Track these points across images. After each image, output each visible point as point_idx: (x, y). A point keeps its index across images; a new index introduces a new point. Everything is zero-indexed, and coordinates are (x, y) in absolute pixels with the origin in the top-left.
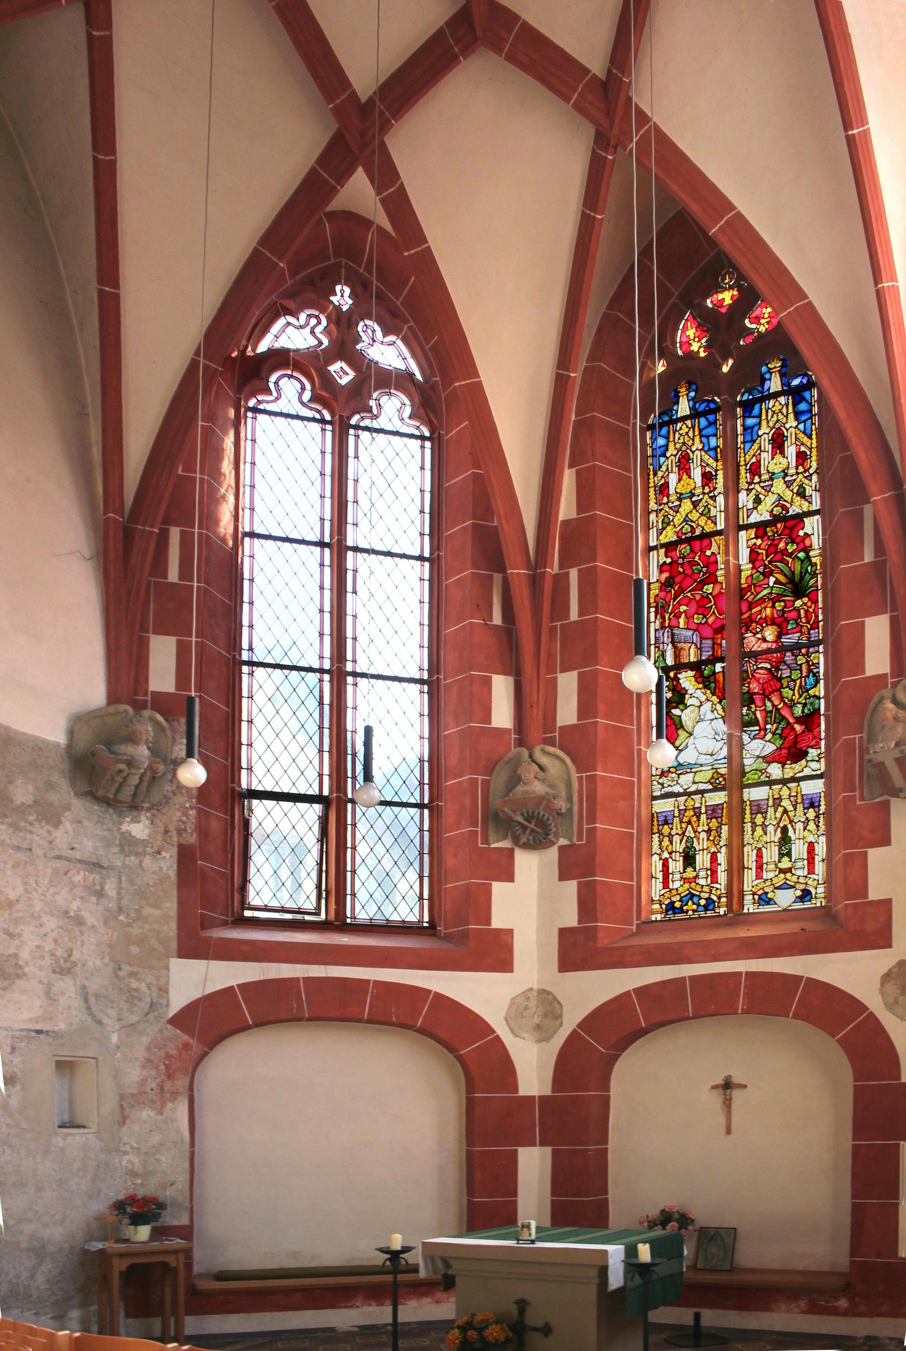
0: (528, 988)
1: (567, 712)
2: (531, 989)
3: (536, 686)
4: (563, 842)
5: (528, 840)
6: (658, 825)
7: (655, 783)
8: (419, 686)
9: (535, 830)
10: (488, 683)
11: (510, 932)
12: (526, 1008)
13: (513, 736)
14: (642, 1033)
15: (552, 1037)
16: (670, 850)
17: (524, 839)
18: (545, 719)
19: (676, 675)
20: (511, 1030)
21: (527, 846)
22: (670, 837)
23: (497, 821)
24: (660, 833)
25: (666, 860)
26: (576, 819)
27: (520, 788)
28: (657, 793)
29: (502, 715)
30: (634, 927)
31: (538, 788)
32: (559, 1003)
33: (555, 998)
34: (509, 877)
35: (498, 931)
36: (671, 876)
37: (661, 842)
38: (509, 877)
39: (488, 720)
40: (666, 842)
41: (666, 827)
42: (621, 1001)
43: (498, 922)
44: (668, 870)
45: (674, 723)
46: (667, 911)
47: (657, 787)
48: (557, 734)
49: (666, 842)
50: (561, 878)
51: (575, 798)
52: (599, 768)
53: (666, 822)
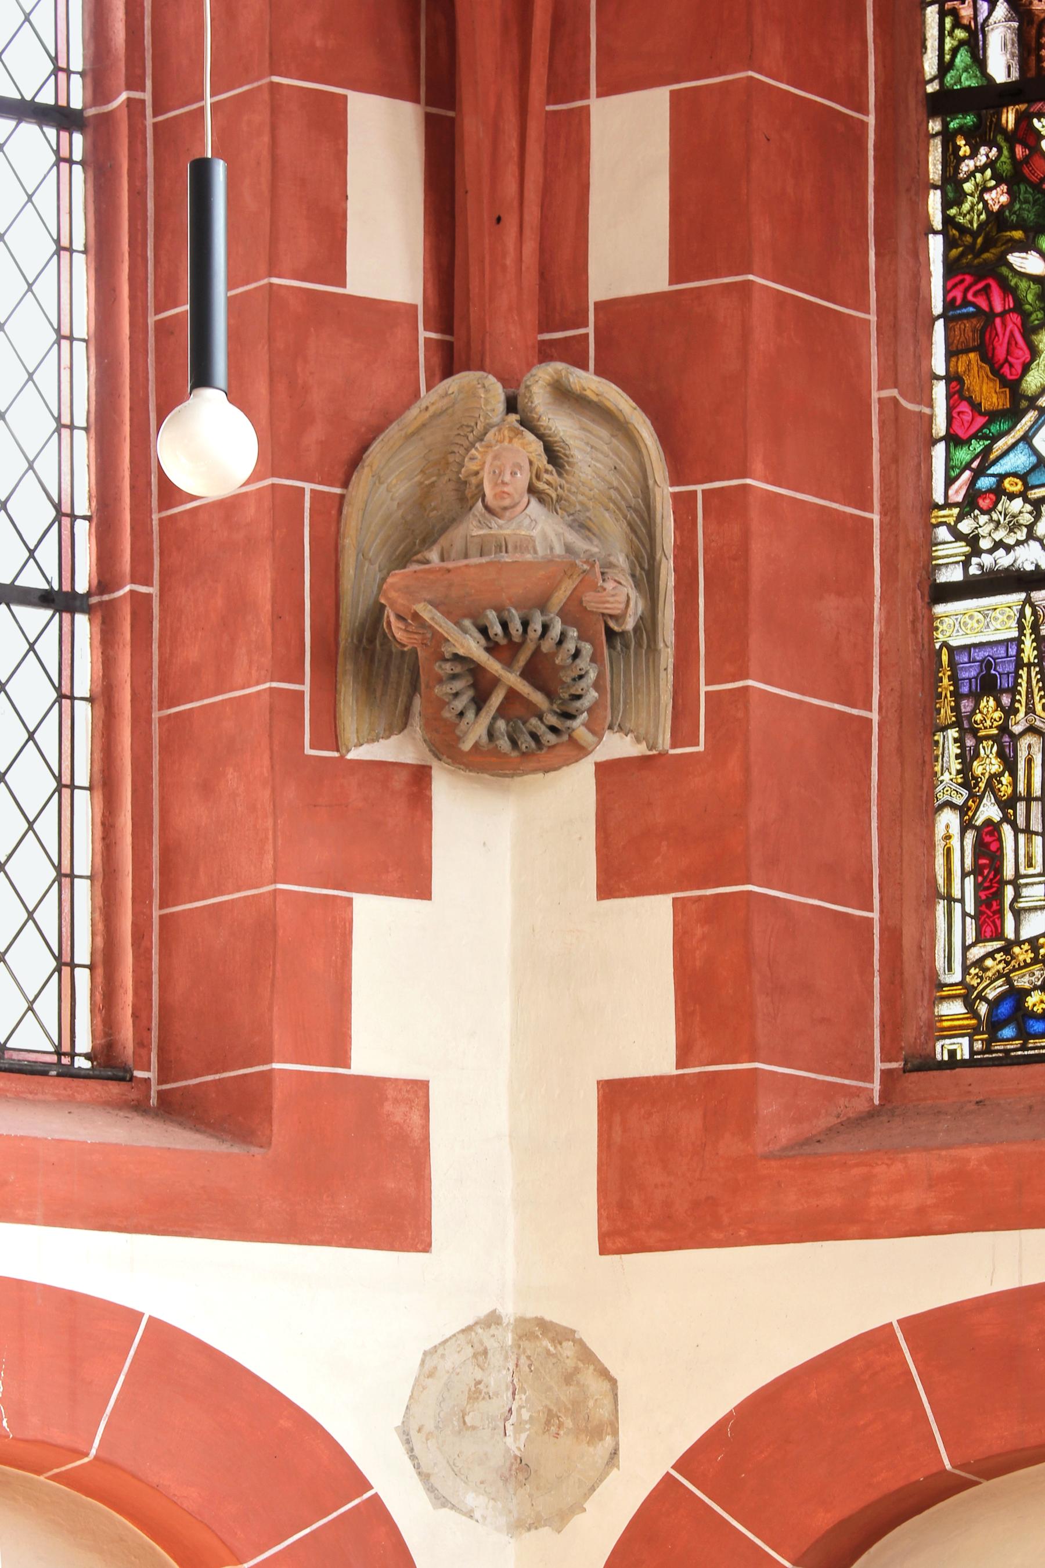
0: (483, 1312)
1: (629, 247)
2: (493, 1320)
3: (513, 144)
4: (618, 746)
5: (491, 734)
6: (957, 695)
7: (943, 533)
8: (51, 132)
9: (517, 696)
10: (330, 124)
11: (420, 1088)
12: (477, 1393)
13: (423, 334)
14: (932, 1492)
15: (578, 1508)
16: (1006, 790)
17: (475, 731)
18: (544, 274)
19: (1024, 119)
20: (425, 1477)
21: (489, 763)
22: (1006, 741)
23: (375, 661)
24: (967, 728)
25: (992, 828)
26: (667, 657)
27: (473, 527)
28: (954, 575)
29: (385, 257)
30: (876, 1086)
31: (540, 530)
32: (604, 1373)
33: (587, 1355)
34: (413, 879)
35: (374, 1088)
36: (1009, 892)
37: (967, 758)
38: (413, 879)
39: (333, 266)
40: (988, 764)
41: (988, 704)
42: (855, 1370)
43: (374, 1050)
44: (999, 869)
45: (1019, 306)
46: (994, 1025)
47: (951, 550)
48: (590, 330)
49: (988, 764)
50: (610, 885)
51: (667, 578)
52: (758, 465)
53: (988, 685)
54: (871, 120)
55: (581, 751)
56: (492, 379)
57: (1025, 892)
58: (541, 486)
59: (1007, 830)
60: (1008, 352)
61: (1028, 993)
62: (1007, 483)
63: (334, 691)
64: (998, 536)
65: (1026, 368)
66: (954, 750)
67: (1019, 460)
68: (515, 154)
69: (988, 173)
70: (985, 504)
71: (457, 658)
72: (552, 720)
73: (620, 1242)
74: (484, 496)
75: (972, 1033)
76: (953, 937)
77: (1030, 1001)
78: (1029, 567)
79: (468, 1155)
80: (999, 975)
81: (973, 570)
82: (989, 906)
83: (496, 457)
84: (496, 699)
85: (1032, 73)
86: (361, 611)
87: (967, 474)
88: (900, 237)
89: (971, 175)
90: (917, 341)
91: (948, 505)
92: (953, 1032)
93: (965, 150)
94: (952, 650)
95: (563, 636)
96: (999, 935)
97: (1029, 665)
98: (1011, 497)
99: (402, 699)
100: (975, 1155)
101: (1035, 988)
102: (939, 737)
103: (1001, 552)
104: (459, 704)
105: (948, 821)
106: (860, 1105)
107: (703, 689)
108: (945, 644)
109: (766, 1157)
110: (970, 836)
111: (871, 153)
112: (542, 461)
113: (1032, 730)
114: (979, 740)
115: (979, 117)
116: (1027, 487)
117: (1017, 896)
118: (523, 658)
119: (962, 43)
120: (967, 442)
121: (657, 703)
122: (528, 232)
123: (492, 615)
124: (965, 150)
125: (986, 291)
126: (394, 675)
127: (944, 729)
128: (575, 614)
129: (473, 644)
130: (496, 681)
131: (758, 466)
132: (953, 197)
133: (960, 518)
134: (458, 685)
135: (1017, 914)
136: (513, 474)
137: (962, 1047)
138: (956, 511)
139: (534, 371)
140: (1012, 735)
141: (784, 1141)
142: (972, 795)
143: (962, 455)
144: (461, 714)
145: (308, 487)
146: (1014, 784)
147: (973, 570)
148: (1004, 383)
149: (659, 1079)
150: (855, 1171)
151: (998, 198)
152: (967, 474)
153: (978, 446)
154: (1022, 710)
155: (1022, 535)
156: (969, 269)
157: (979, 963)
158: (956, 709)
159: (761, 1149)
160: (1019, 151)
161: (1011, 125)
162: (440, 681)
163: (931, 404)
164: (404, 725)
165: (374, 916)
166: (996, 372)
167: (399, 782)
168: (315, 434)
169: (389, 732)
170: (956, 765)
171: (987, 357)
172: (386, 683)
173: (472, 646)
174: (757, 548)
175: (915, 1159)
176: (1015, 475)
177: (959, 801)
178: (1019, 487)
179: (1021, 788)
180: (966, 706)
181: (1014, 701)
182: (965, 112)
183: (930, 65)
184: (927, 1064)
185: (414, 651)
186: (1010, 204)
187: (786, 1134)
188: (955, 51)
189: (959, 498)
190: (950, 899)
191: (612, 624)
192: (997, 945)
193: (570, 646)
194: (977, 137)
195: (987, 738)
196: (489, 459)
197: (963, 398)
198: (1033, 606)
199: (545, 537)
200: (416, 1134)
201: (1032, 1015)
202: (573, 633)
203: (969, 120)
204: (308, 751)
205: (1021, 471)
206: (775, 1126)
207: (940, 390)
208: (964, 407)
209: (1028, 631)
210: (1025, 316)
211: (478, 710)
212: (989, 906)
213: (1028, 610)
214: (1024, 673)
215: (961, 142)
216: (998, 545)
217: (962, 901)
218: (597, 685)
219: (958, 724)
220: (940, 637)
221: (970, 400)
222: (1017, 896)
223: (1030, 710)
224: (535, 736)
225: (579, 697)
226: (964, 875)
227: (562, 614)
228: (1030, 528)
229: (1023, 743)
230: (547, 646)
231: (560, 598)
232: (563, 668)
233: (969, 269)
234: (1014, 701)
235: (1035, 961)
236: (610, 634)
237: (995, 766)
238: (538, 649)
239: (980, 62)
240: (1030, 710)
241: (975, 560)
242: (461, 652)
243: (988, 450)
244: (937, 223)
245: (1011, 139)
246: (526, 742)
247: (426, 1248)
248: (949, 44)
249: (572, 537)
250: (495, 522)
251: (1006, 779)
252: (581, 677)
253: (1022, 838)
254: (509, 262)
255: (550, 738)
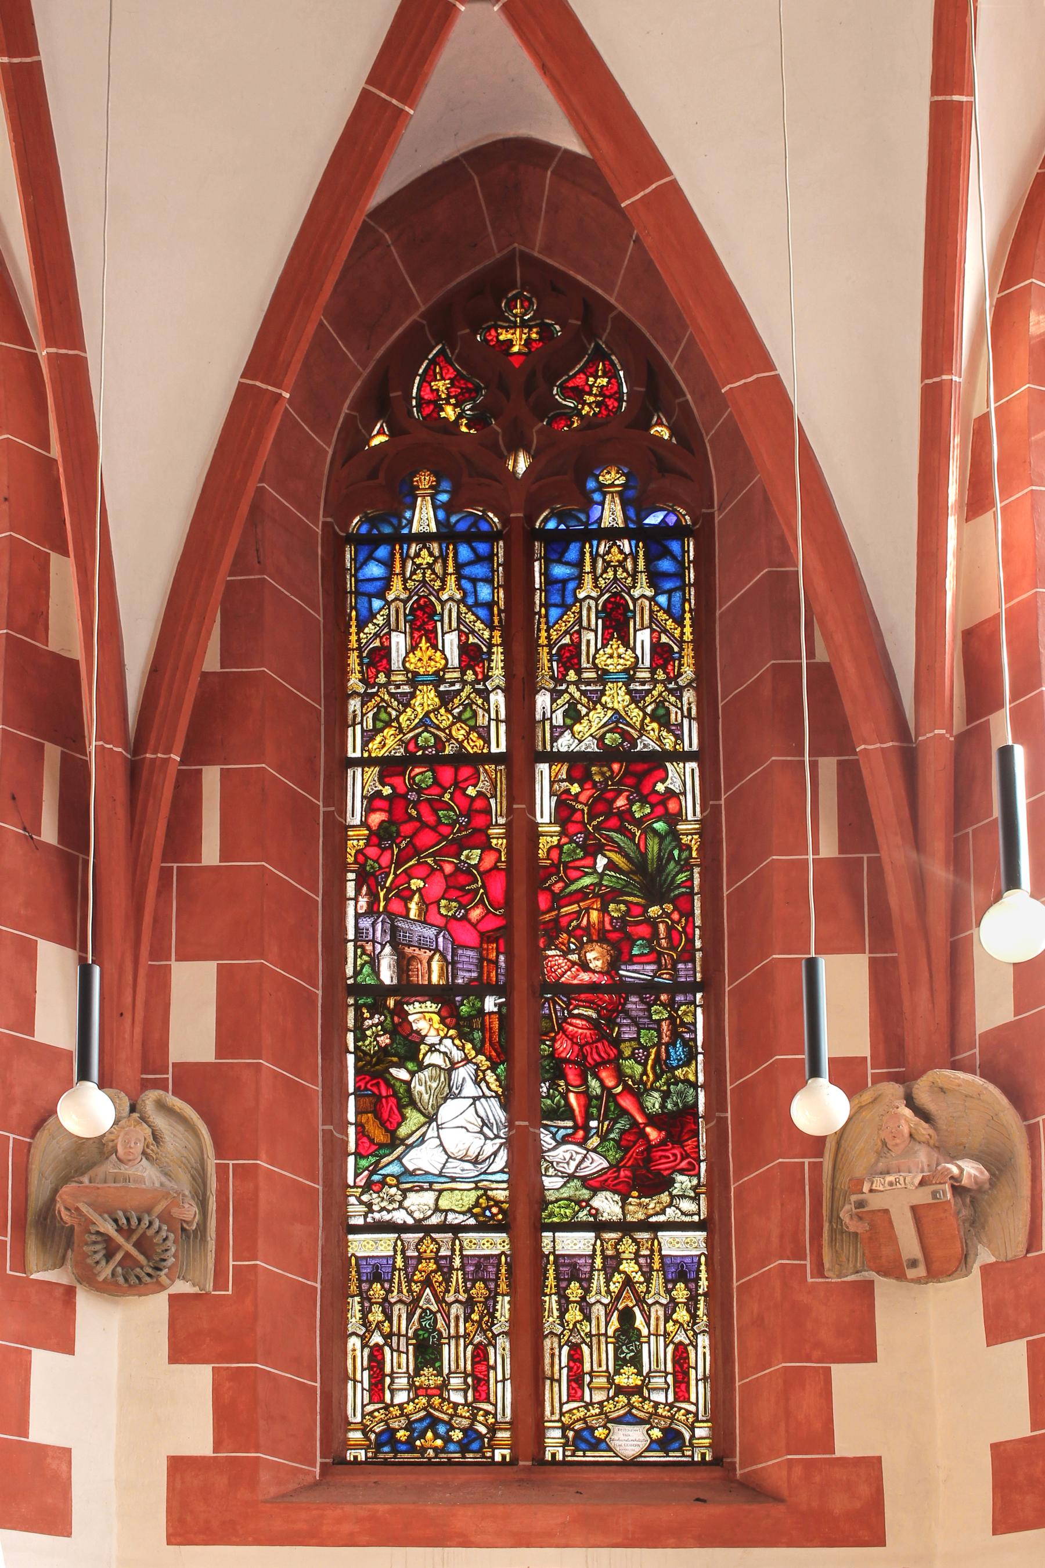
3: (130, 978)
4: (182, 1287)
5: (113, 1274)
9: (130, 1256)
18: (144, 1044)
21: (109, 1289)
25: (377, 1350)
26: (212, 1245)
27: (110, 1167)
30: (318, 1470)
31: (148, 1174)
34: (66, 1344)
35: (41, 1450)
36: (388, 1380)
37: (365, 1313)
38: (66, 1344)
41: (377, 1286)
43: (42, 1430)
44: (382, 1368)
45: (395, 1094)
46: (379, 1445)
48: (170, 1076)
49: (377, 1315)
51: (212, 1205)
54: (320, 992)
55: (163, 1288)
56: (122, 1094)
57: (396, 1381)
58: (149, 1151)
59: (387, 1349)
60: (389, 1116)
61: (398, 1430)
62: (388, 1179)
63: (24, 1242)
64: (383, 1204)
65: (399, 1125)
66: (358, 1307)
67: (395, 1169)
68: (131, 982)
69: (379, 1027)
70: (376, 1188)
71: (98, 1233)
72: (150, 1271)
73: (179, 1539)
74: (116, 1152)
75: (366, 1448)
76: (356, 1398)
77: (398, 1435)
78: (400, 1222)
79: (90, 1487)
80: (382, 1421)
81: (369, 1220)
82: (376, 1386)
83: (126, 1134)
84: (119, 1256)
85: (404, 982)
86: (40, 1203)
87: (366, 1173)
88: (334, 1052)
89: (370, 1027)
90: (341, 1104)
91: (355, 1186)
92: (357, 1447)
93: (367, 1015)
94: (357, 1258)
95: (160, 1228)
96: (382, 1401)
97: (400, 1270)
98: (391, 1186)
99: (61, 1251)
100: (382, 1508)
101: (401, 1428)
102: (350, 1300)
103: (385, 1213)
104: (98, 1257)
105: (354, 1342)
106: (309, 1479)
107: (231, 1263)
108: (353, 1255)
109: (265, 1502)
110: (366, 1351)
111: (320, 1009)
112: (151, 1140)
113: (400, 1301)
114: (372, 1304)
115: (374, 999)
116: (399, 1183)
117: (591, 1381)
118: (135, 1237)
119: (366, 962)
120: (367, 1157)
121: (206, 1267)
122: (137, 1023)
123: (120, 1213)
124: (367, 1015)
125: (378, 1085)
126: (57, 1238)
127: (353, 1296)
128: (166, 1217)
129: (110, 1227)
130: (119, 1247)
131: (264, 1155)
132: (360, 1037)
133: (362, 1194)
134: (98, 1247)
135: (392, 1392)
136: (136, 1143)
137: (361, 1455)
138: (360, 1190)
139: (147, 1093)
140: (390, 1303)
141: (272, 1494)
142: (367, 1331)
143: (364, 1163)
144: (97, 1263)
145: (12, 1136)
146: (391, 1327)
147: (369, 1220)
148: (387, 1130)
149: (203, 1458)
150: (314, 1512)
151: (384, 1040)
152: (366, 1173)
153: (373, 1160)
154: (396, 1291)
155: (396, 1205)
156: (368, 1073)
157: (371, 1414)
158: (359, 1287)
159: (261, 1497)
160: (396, 1019)
161: (392, 1006)
162: (87, 1244)
163: (347, 1135)
164: (62, 1264)
165: (43, 1362)
166: (383, 1124)
167: (58, 1293)
168: (16, 1110)
169: (54, 1267)
170: (359, 1315)
171: (378, 1116)
172: (52, 1241)
173: (110, 1229)
174: (262, 1195)
175: (349, 1509)
176: (392, 1176)
177: (361, 1333)
178: (395, 1182)
179: (395, 1329)
180: (365, 1286)
181: (391, 1286)
182: (368, 997)
183: (349, 971)
184: (344, 1462)
185: (72, 1228)
186: (391, 1044)
187: (273, 1491)
188: (363, 966)
189: (362, 1184)
190: (355, 1381)
191: (185, 1225)
192: (381, 1405)
193: (164, 1234)
194: (374, 1010)
195: (376, 1303)
196: (122, 1134)
197: (364, 1135)
198: (402, 1241)
199: (150, 1177)
200: (64, 1476)
201: (400, 1441)
202: (165, 1227)
203: (369, 1001)
204: (8, 1272)
205: (396, 1174)
206: (268, 1486)
207: (352, 1130)
208: (365, 1140)
209: (399, 1253)
210: (399, 1099)
211: (107, 1262)
212: (376, 1386)
213: (399, 1243)
214: (396, 1273)
215: (365, 1011)
216: (383, 1209)
217: (362, 1382)
218: (174, 1256)
219: (360, 1294)
220: (351, 1251)
221: (368, 1137)
222: (392, 1382)
223: (400, 1291)
224: (138, 1277)
225: (164, 1260)
226: (363, 1370)
227: (158, 1217)
228: (401, 1203)
229: (396, 1308)
230: (150, 1233)
231: (159, 1208)
232: (157, 1244)
233: (368, 1073)
234: (391, 1286)
235: (401, 1415)
236: (183, 1229)
237: (381, 1317)
238: (144, 1233)
239: (376, 972)
240: (400, 1291)
241: (370, 1215)
242: (102, 1230)
243: (377, 1162)
244: (351, 1048)
245: (392, 1013)
246: (133, 1280)
247: (69, 1534)
248: (359, 962)
249: (164, 1179)
250: (123, 1167)
251: (386, 1324)
252: (167, 1250)
253: (395, 1354)
254: (127, 1036)
255: (148, 1279)
